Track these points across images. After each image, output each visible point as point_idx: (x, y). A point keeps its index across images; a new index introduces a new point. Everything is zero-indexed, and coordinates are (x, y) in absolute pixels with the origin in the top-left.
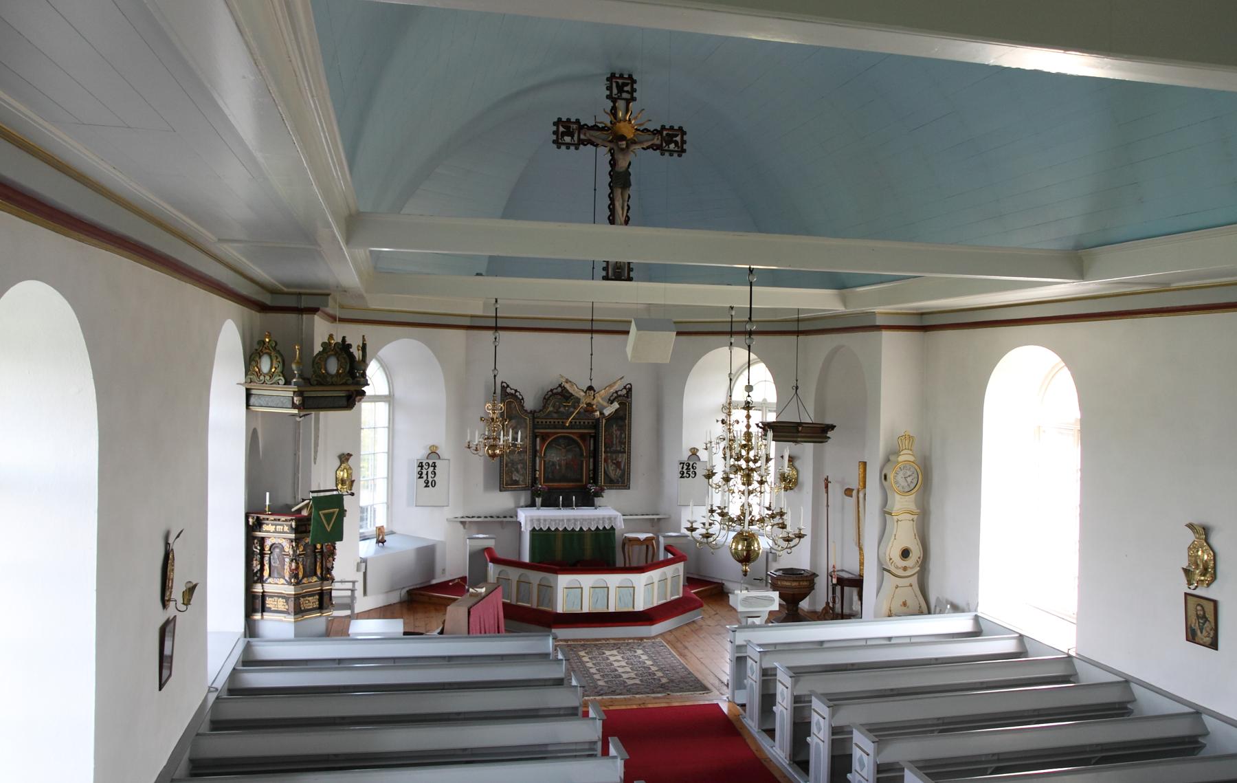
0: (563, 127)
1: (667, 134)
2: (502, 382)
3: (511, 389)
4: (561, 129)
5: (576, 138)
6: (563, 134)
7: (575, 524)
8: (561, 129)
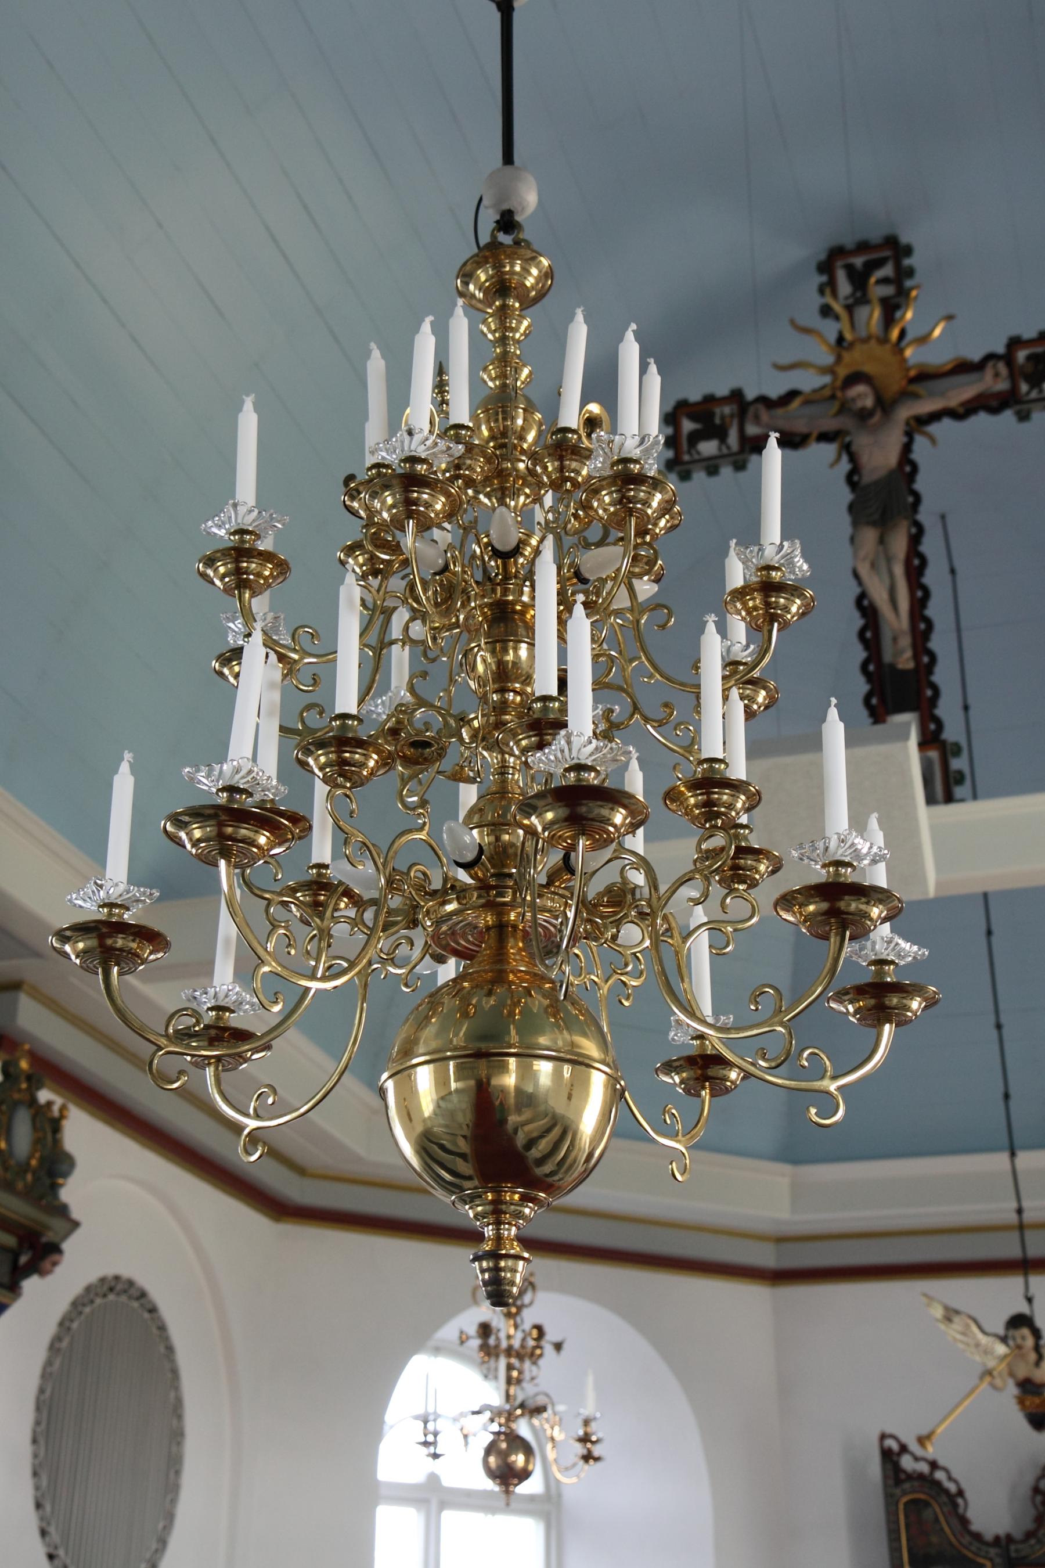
0: (693, 418)
1: (1029, 358)
2: (883, 1437)
3: (917, 1459)
4: (688, 426)
5: (733, 439)
6: (695, 438)
7: (582, 1469)
8: (688, 426)
